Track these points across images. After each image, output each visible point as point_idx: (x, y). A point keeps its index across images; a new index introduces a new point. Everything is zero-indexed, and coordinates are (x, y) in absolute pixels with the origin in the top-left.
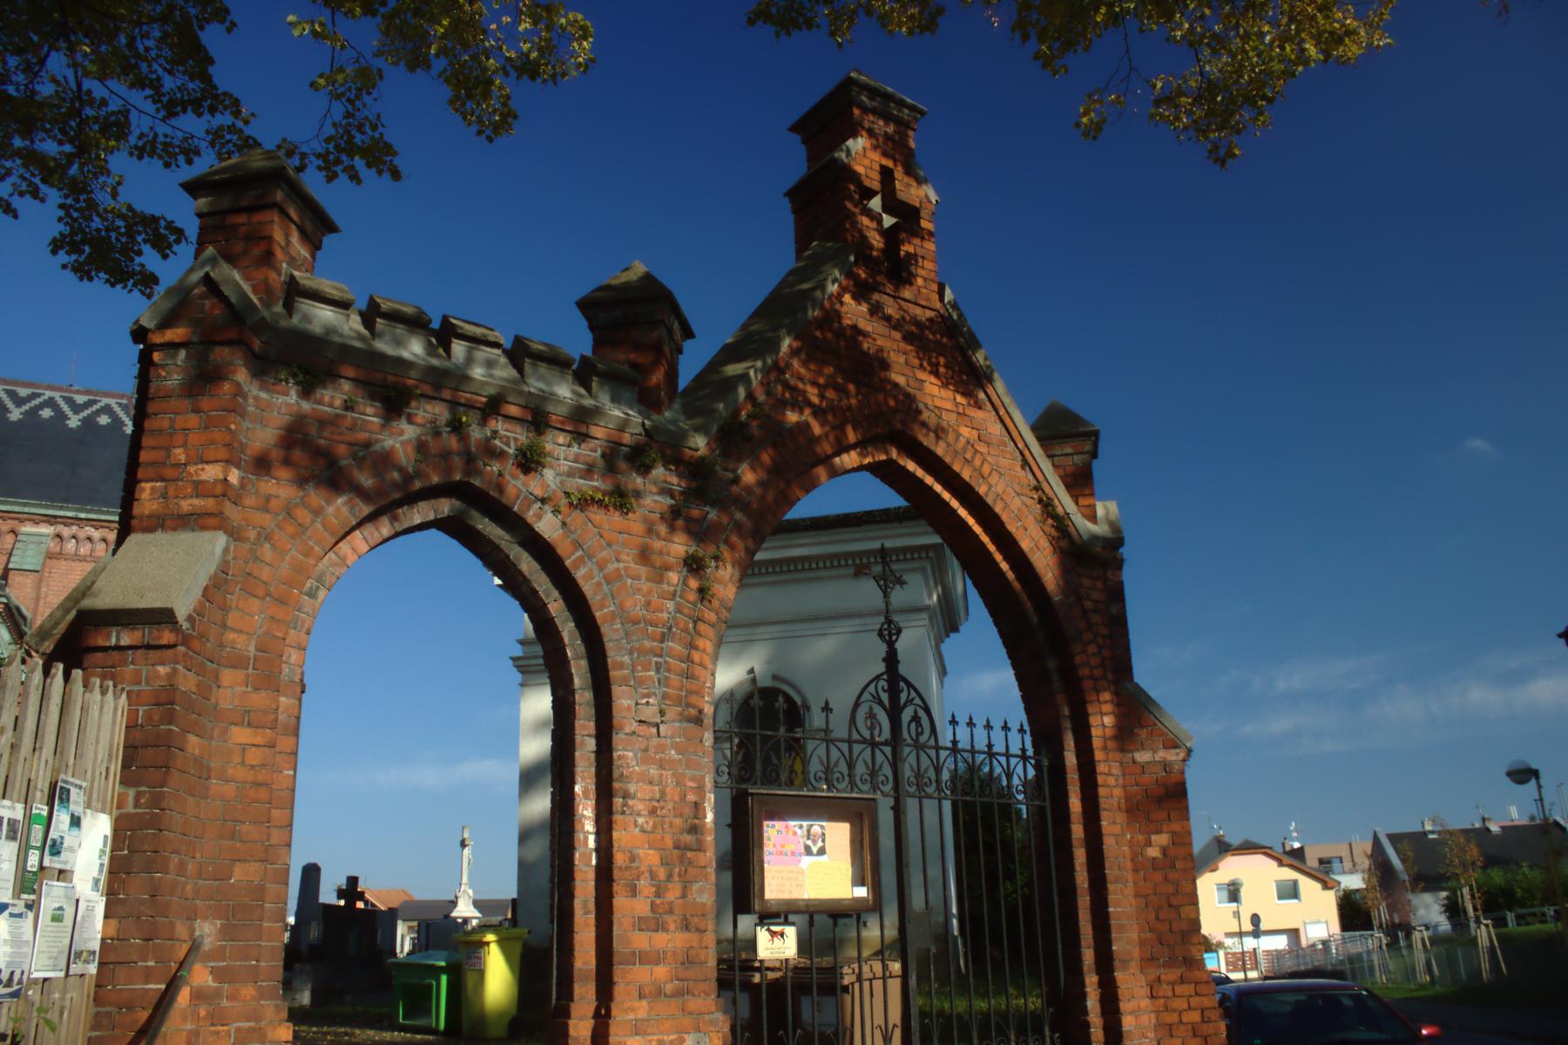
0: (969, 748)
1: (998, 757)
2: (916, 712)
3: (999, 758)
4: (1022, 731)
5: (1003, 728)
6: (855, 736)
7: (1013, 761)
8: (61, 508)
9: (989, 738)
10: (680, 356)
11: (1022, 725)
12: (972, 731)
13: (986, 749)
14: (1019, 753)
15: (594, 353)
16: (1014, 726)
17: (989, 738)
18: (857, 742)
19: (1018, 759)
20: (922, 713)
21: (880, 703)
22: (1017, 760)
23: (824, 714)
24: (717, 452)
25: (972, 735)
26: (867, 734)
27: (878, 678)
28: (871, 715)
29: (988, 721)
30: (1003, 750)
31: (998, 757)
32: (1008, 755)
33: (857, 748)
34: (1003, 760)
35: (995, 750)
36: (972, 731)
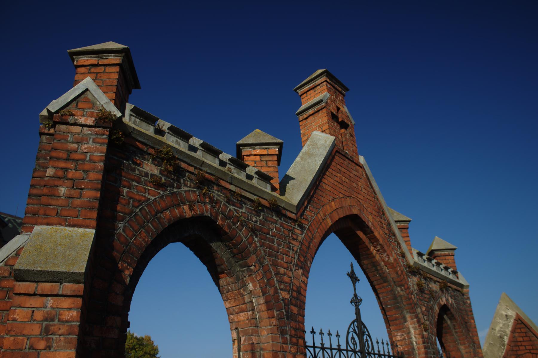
0: (312, 345)
1: (309, 348)
2: (353, 335)
3: (343, 352)
4: (387, 344)
5: (311, 332)
6: (349, 349)
7: (317, 350)
8: (339, 87)
9: (322, 339)
10: (130, 95)
11: (387, 341)
12: (313, 336)
13: (337, 347)
14: (320, 346)
15: (237, 157)
16: (385, 342)
17: (322, 339)
18: (350, 351)
19: (336, 351)
20: (368, 338)
21: (355, 332)
22: (319, 349)
23: (312, 335)
24: (114, 118)
25: (313, 338)
26: (352, 347)
27: (353, 322)
28: (353, 338)
29: (313, 329)
30: (329, 346)
31: (309, 348)
32: (314, 347)
33: (350, 353)
34: (312, 350)
35: (325, 346)
36: (313, 336)
